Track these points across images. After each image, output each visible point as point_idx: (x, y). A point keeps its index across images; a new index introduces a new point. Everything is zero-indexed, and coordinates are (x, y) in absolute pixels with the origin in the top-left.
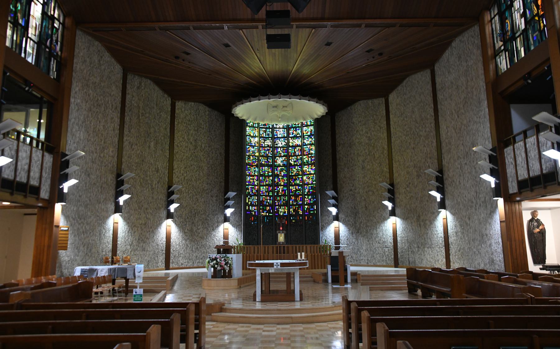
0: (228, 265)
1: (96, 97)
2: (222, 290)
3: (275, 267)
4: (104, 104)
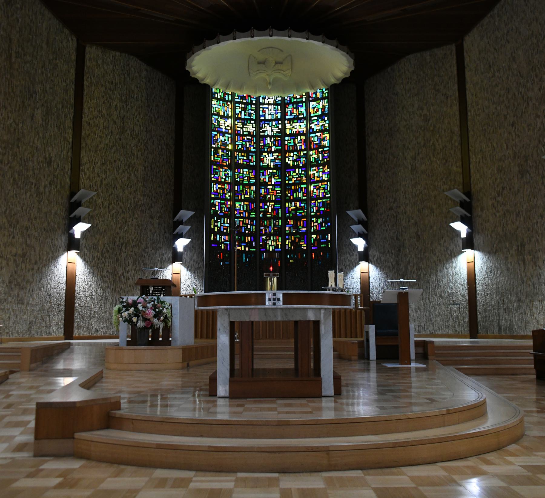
0: (162, 318)
2: (147, 370)
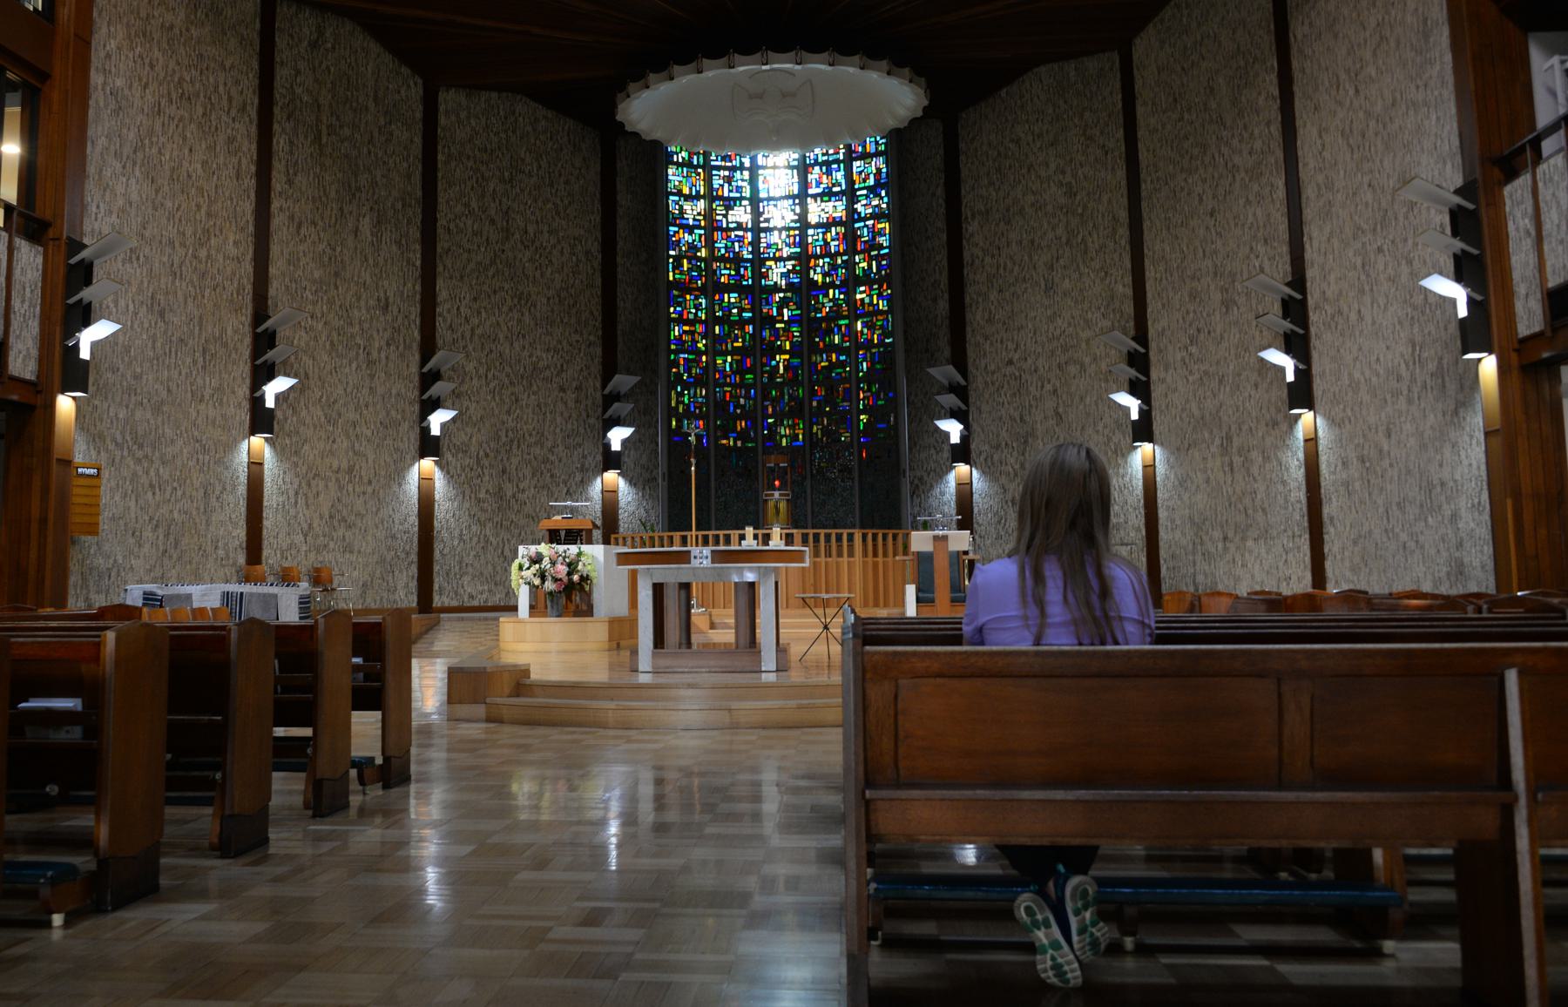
1: (174, 71)
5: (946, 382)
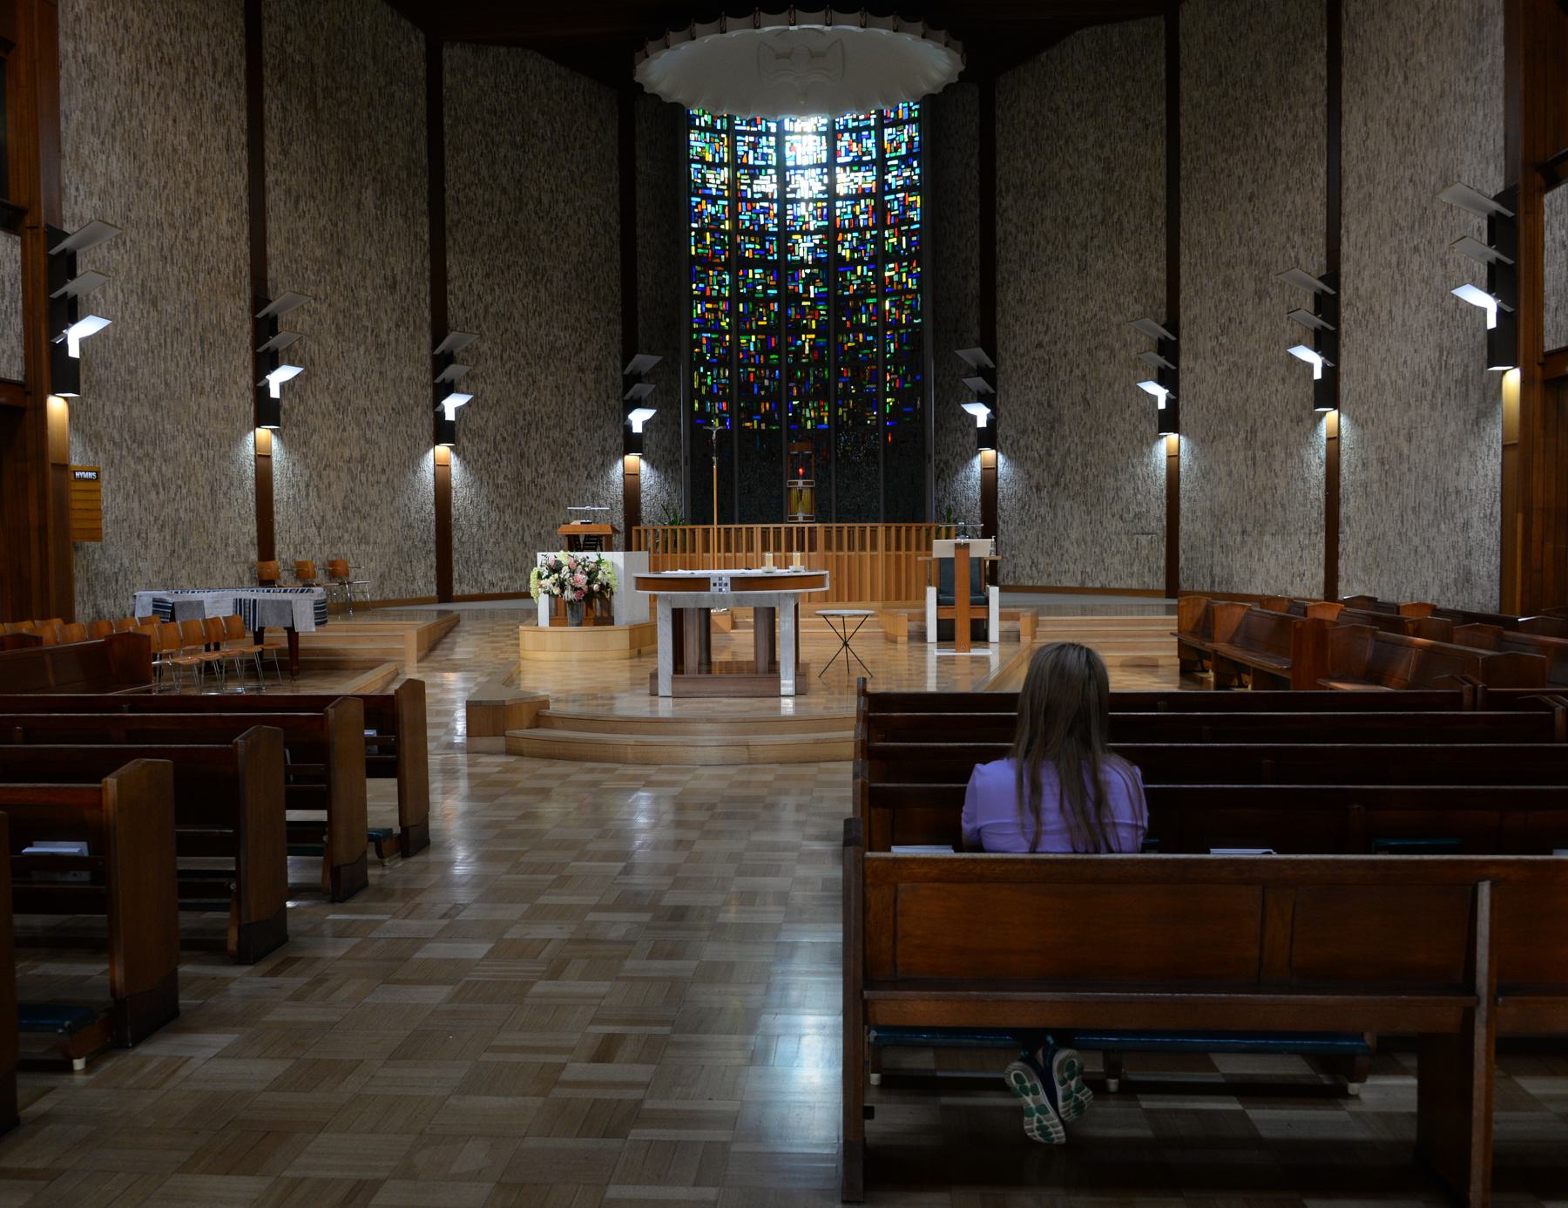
1: (151, 33)
3: (714, 590)
4: (183, 58)
5: (974, 365)
